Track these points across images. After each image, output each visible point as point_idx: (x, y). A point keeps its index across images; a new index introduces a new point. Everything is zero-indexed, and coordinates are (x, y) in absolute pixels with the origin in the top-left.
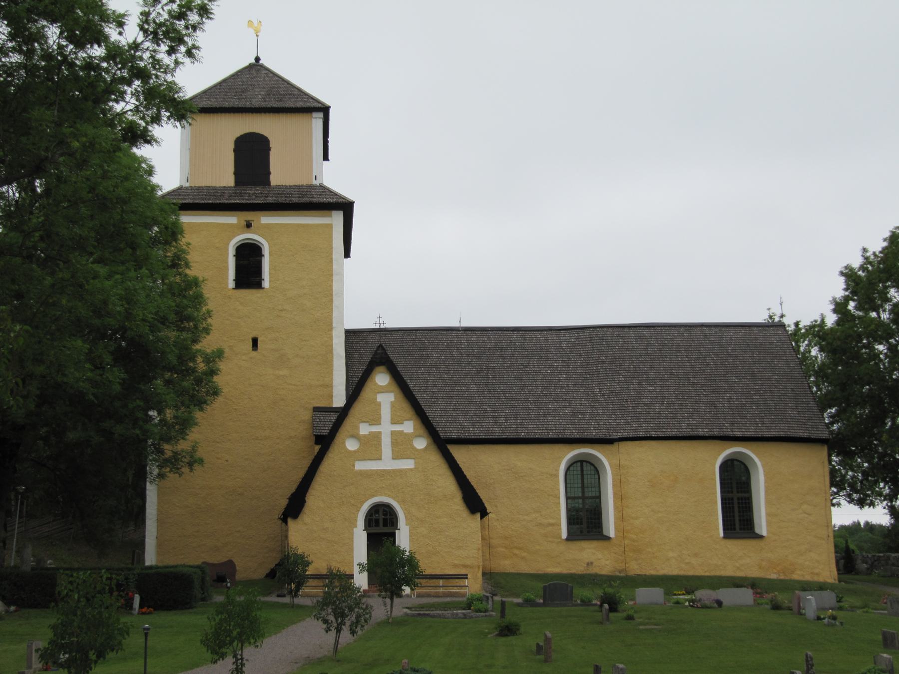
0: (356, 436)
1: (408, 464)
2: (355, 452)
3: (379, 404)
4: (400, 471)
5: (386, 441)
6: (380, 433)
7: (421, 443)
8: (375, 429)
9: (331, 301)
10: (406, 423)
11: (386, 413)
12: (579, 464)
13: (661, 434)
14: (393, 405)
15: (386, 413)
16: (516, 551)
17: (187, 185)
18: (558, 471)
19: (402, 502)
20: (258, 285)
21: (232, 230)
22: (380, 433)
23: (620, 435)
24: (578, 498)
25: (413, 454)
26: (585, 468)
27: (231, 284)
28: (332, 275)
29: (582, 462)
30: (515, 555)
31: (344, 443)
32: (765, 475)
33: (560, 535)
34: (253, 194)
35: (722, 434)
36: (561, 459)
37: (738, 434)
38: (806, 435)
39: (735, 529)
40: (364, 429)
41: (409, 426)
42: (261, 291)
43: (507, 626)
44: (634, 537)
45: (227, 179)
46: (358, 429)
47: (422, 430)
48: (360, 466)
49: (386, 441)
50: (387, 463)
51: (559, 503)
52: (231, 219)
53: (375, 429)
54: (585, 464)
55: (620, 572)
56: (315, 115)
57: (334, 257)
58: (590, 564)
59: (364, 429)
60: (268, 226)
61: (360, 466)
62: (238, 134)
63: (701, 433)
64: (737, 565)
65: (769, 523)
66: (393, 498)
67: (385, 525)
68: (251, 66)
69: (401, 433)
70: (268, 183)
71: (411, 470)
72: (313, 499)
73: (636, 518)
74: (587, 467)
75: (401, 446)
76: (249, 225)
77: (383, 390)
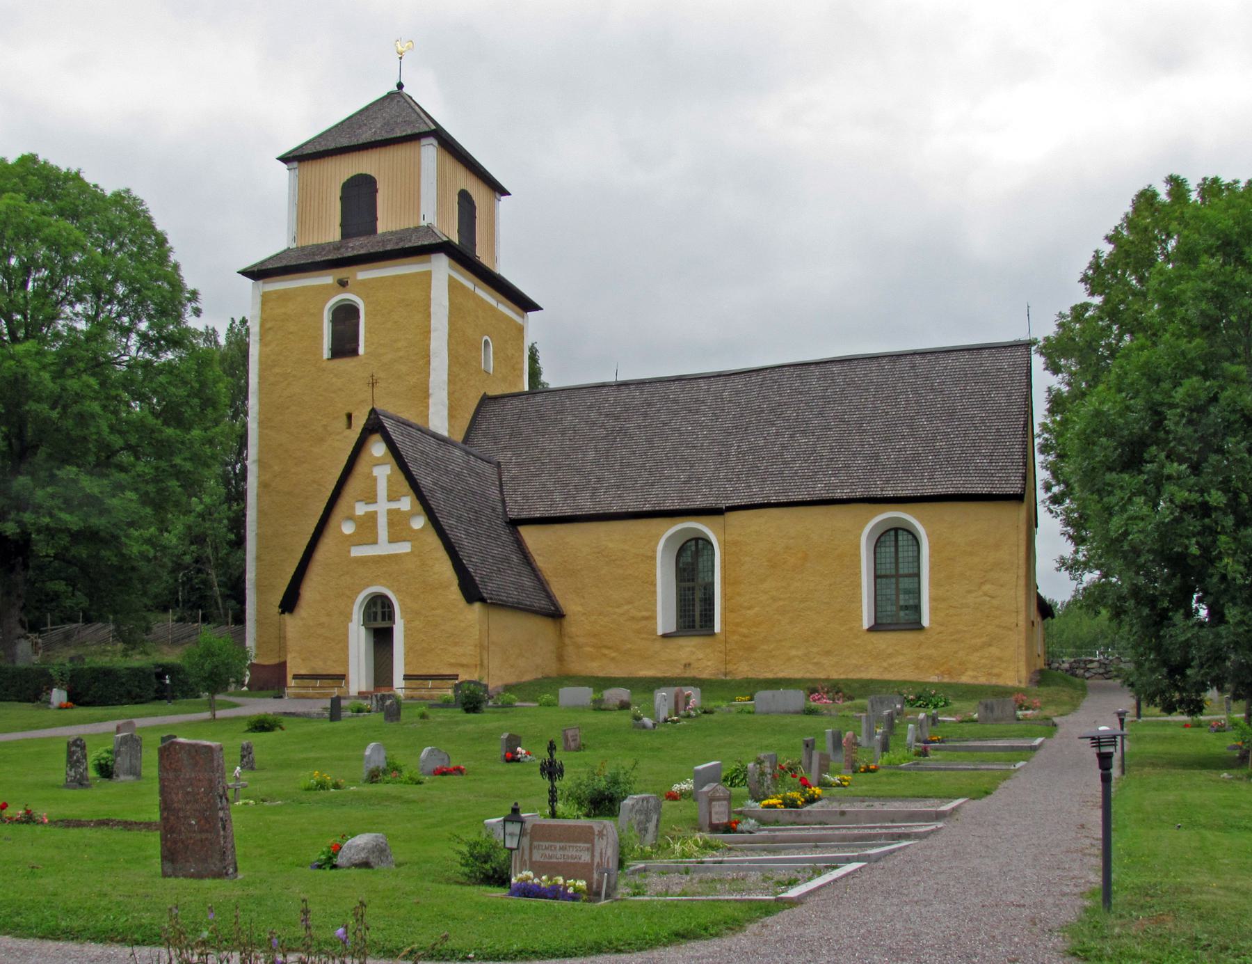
0: (350, 518)
1: (404, 548)
2: (350, 535)
3: (375, 479)
4: (397, 555)
5: (382, 522)
6: (376, 513)
7: (419, 523)
8: (371, 508)
9: (428, 363)
10: (403, 499)
11: (382, 489)
12: (892, 533)
13: (783, 499)
14: (389, 479)
15: (382, 489)
16: (606, 651)
17: (294, 246)
18: (655, 551)
19: (396, 592)
20: (355, 352)
21: (325, 292)
22: (376, 513)
23: (730, 503)
24: (892, 576)
25: (411, 536)
26: (900, 538)
27: (326, 353)
28: (430, 332)
29: (896, 530)
30: (605, 655)
31: (340, 527)
32: (930, 547)
33: (655, 630)
34: (359, 246)
35: (866, 495)
36: (658, 537)
37: (889, 493)
38: (985, 490)
39: (694, 627)
40: (361, 509)
41: (406, 503)
42: (355, 359)
43: (75, 741)
44: (745, 631)
45: (333, 234)
46: (354, 508)
47: (419, 508)
48: (357, 552)
49: (382, 522)
50: (383, 548)
51: (655, 592)
52: (327, 279)
53: (371, 508)
54: (900, 532)
55: (726, 675)
56: (424, 141)
57: (432, 309)
58: (687, 665)
59: (361, 509)
60: (364, 283)
61: (357, 552)
62: (346, 177)
63: (838, 494)
64: (885, 664)
65: (933, 610)
66: (389, 588)
67: (383, 619)
68: (390, 95)
69: (398, 511)
70: (374, 231)
71: (407, 554)
72: (309, 592)
73: (749, 608)
74: (902, 537)
75: (398, 526)
76: (343, 284)
77: (379, 462)
